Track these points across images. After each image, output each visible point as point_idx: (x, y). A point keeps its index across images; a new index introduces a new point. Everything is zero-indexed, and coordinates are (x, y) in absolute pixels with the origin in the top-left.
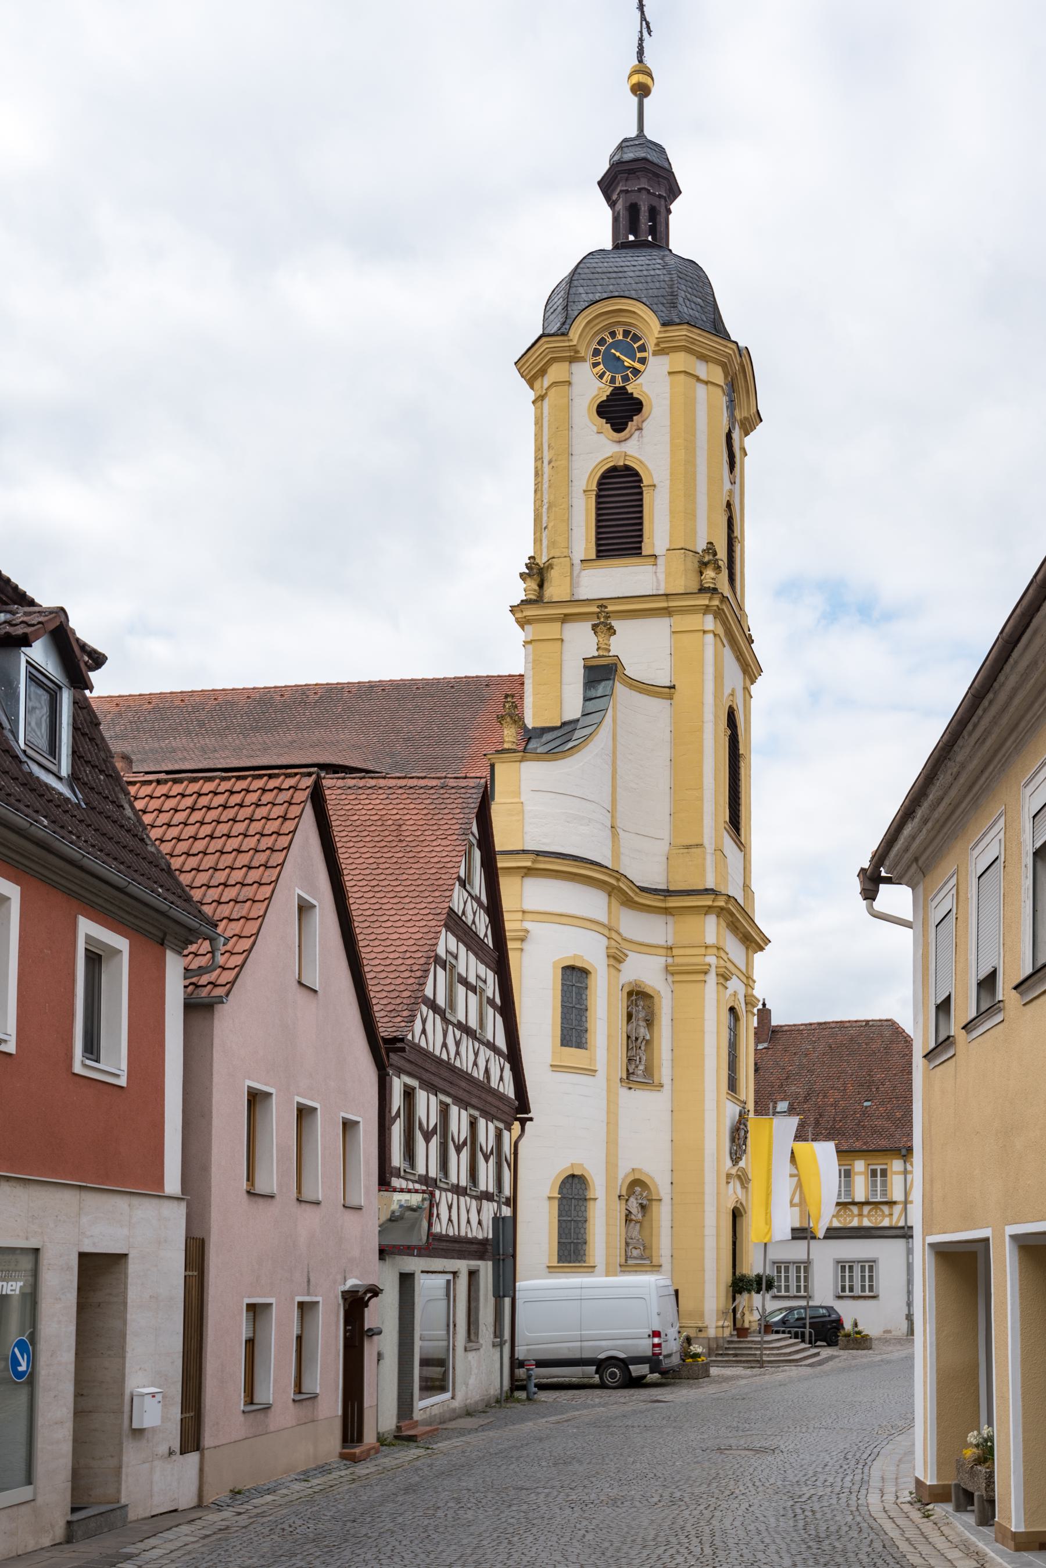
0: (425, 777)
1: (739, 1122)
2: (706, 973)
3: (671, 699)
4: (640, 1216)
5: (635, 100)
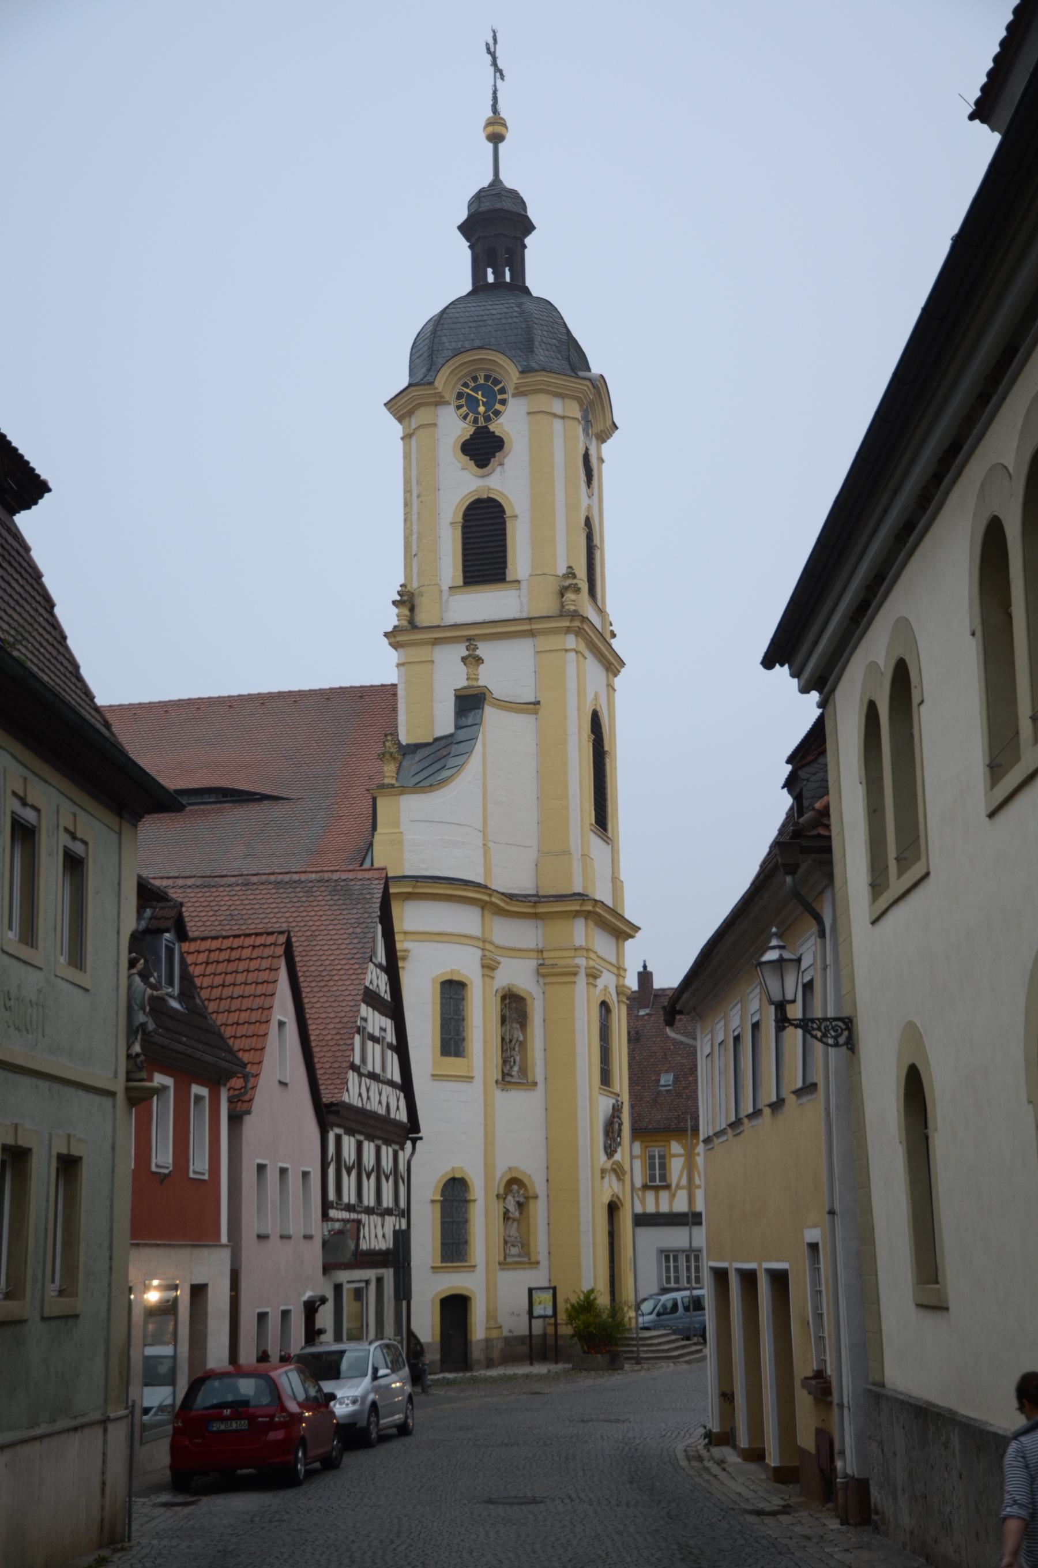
0: (336, 871)
1: (613, 1116)
2: (575, 974)
3: (537, 713)
4: (517, 1214)
5: (490, 146)
